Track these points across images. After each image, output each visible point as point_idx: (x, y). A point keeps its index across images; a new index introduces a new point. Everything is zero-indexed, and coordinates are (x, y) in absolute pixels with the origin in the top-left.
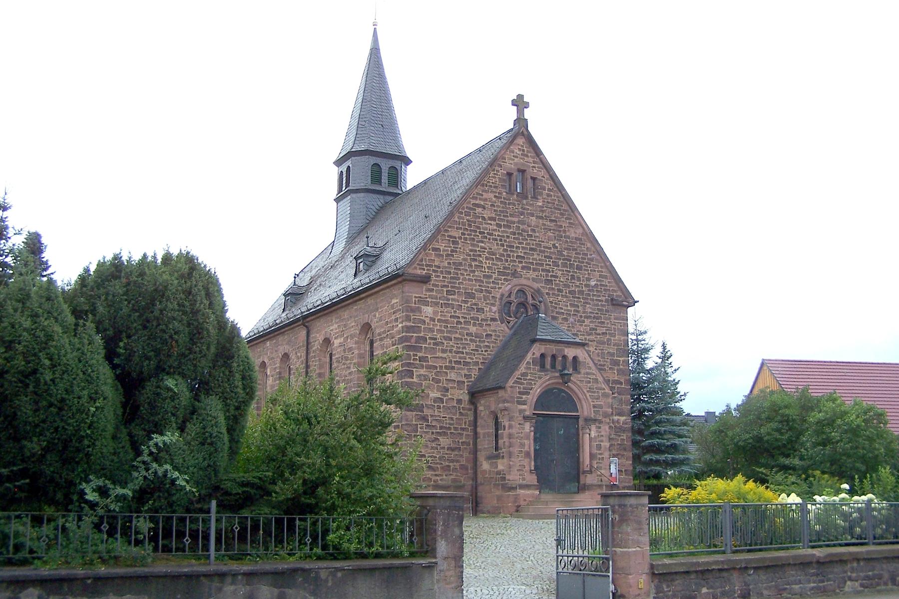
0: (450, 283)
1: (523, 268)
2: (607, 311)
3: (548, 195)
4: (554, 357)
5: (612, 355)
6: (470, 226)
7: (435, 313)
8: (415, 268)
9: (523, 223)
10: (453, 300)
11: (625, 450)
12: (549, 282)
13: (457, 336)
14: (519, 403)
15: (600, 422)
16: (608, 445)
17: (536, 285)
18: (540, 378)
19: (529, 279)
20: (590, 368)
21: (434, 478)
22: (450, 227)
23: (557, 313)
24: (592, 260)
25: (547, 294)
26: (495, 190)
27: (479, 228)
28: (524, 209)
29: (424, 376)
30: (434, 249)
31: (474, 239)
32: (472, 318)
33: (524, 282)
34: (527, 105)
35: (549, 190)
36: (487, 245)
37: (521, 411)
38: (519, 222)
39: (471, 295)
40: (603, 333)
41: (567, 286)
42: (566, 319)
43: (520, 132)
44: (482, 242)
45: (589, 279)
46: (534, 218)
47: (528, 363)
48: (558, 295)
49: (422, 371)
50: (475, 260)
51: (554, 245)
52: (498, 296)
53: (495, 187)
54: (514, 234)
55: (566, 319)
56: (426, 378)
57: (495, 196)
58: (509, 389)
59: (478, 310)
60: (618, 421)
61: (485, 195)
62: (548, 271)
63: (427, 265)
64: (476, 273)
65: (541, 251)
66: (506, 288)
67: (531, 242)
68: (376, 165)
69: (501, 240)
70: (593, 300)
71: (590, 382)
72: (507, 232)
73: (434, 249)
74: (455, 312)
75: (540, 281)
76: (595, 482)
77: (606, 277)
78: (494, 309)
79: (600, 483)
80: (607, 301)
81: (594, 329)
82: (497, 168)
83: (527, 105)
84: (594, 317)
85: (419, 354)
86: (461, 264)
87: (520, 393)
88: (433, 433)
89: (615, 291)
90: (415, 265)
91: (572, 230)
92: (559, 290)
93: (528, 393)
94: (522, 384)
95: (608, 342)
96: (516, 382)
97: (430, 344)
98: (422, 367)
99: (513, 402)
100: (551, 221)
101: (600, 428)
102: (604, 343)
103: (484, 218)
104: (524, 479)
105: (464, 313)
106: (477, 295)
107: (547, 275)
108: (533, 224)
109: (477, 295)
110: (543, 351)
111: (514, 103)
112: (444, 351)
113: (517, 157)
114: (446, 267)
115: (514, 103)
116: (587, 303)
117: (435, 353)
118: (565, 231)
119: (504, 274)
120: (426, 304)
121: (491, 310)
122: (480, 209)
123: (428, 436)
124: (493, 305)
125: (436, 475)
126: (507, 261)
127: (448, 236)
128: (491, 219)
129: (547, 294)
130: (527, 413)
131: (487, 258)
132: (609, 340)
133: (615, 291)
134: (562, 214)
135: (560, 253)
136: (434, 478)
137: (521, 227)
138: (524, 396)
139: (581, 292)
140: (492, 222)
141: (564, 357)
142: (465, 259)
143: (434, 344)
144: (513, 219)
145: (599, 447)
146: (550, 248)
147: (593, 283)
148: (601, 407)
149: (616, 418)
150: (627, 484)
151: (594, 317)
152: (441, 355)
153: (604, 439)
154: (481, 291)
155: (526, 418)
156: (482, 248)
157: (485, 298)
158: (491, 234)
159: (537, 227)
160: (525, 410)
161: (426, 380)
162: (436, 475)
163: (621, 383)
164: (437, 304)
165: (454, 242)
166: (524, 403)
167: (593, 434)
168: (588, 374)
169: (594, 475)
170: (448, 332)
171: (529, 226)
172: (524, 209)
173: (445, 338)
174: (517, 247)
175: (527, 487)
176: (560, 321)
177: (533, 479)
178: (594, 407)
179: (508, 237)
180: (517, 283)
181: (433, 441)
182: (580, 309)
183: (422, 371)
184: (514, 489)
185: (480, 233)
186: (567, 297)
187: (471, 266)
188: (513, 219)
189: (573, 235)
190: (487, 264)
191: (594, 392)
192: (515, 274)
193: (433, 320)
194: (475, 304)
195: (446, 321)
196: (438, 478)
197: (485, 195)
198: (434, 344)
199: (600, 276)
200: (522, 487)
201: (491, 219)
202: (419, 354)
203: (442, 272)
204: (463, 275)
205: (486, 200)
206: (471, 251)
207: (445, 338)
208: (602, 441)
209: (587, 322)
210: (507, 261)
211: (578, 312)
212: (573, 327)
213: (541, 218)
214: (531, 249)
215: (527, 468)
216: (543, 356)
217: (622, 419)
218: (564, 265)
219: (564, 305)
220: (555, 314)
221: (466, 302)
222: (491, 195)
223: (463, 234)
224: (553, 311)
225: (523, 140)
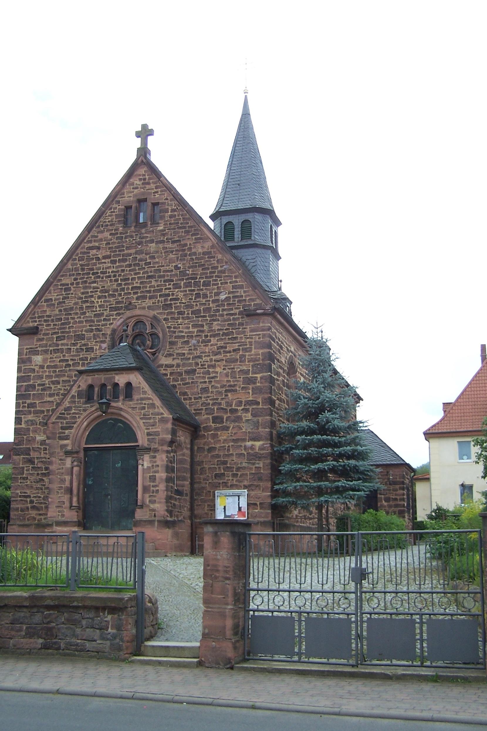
0: (61, 329)
1: (138, 299)
2: (241, 324)
3: (171, 217)
4: (103, 386)
5: (247, 372)
6: (83, 270)
7: (45, 360)
8: (28, 322)
9: (140, 252)
10: (62, 344)
11: (260, 479)
12: (167, 306)
13: (66, 378)
14: (61, 438)
15: (156, 450)
16: (164, 475)
17: (152, 313)
18: (85, 410)
19: (144, 309)
20: (145, 393)
21: (38, 517)
22: (62, 276)
23: (176, 337)
24: (223, 272)
25: (165, 319)
26: (110, 228)
27: (92, 269)
28: (143, 238)
29: (32, 421)
30: (47, 301)
31: (86, 282)
32: (81, 359)
33: (137, 312)
34: (151, 133)
35: (173, 210)
36: (99, 285)
37: (63, 446)
38: (136, 253)
39: (81, 337)
40: (234, 350)
41: (188, 306)
42: (187, 342)
43: (143, 162)
44: (95, 282)
45: (218, 294)
46: (154, 244)
47: (73, 397)
48: (179, 318)
49: (30, 417)
50: (87, 301)
51: (177, 268)
52: (109, 332)
53: (111, 225)
54: (130, 266)
55: (187, 342)
56: (33, 423)
57: (111, 234)
58: (51, 425)
59: (88, 350)
60: (252, 447)
61: (100, 236)
62: (168, 295)
63: (39, 317)
64: (87, 315)
65: (160, 277)
66: (118, 322)
67: (149, 270)
68: (229, 223)
69: (115, 276)
70: (222, 315)
71: (144, 408)
72: (122, 266)
73: (47, 301)
74: (64, 356)
75: (158, 307)
76: (146, 517)
77: (241, 287)
78: (104, 346)
79: (153, 518)
80: (240, 313)
81: (222, 347)
82: (115, 206)
83: (151, 133)
84: (224, 334)
85: (28, 401)
86: (72, 309)
87: (62, 428)
88: (38, 474)
89: (253, 300)
90: (28, 319)
91: (199, 246)
92: (180, 313)
93: (71, 428)
94: (65, 418)
95: (242, 359)
96: (58, 418)
97: (38, 390)
98: (30, 412)
99: (54, 439)
100: (174, 242)
101: (155, 457)
102: (236, 360)
103: (98, 259)
104: (63, 516)
105: (72, 356)
106: (87, 335)
107: (166, 300)
108: (152, 250)
109: (87, 335)
110: (90, 382)
111: (138, 135)
112: (51, 395)
113: (137, 188)
114: (57, 315)
115: (138, 135)
116: (214, 320)
117: (43, 399)
118: (190, 249)
119: (116, 309)
120: (36, 353)
121: (100, 348)
122: (94, 251)
123: (34, 477)
124: (102, 342)
125: (40, 515)
126: (120, 295)
127: (61, 285)
128: (104, 257)
129: (165, 319)
130: (69, 448)
131: (99, 297)
132: (242, 356)
133: (253, 300)
134: (186, 232)
135: (183, 273)
136: (38, 517)
137: (138, 257)
138: (67, 431)
139: (208, 310)
140: (107, 261)
141: (116, 385)
142: (76, 304)
143: (42, 390)
144: (130, 251)
145: (153, 479)
146: (172, 271)
147: (223, 297)
148: (157, 434)
149: (249, 444)
150: (262, 520)
151: (224, 334)
152: (49, 399)
153: (159, 469)
154: (92, 330)
155: (68, 453)
156: (94, 288)
157: (95, 336)
158: (105, 273)
159: (157, 252)
160: (66, 445)
161: (33, 424)
162: (40, 515)
163: (258, 403)
164: (46, 352)
165: (66, 290)
166: (67, 438)
167: (146, 465)
168: (142, 399)
169: (145, 509)
170: (57, 376)
171: (146, 254)
172: (143, 238)
173: (53, 383)
174: (133, 279)
175: (65, 523)
176: (179, 345)
177: (72, 516)
178: (148, 434)
179: (123, 271)
180: (130, 315)
181: (37, 482)
182: (206, 328)
183: (30, 417)
184: (50, 525)
185: (93, 274)
186: (188, 318)
187: (82, 308)
188: (130, 251)
189: (200, 250)
190: (97, 302)
191: (150, 418)
192: (129, 306)
193: (42, 367)
194: (84, 345)
195: (55, 366)
196: (42, 517)
197: (100, 236)
198: (42, 390)
199: (233, 287)
200: (59, 524)
201: (104, 257)
202: (28, 401)
203: (53, 321)
204: (73, 318)
205: (101, 240)
206: (83, 293)
207: (53, 383)
208: (157, 472)
209: (213, 341)
210: (120, 295)
211: (203, 331)
212: (196, 349)
213: (163, 242)
214: (149, 277)
215: (67, 504)
216: (91, 387)
217: (258, 444)
218: (187, 285)
219: (185, 327)
220: (173, 340)
221: (74, 345)
222: (107, 234)
223: (75, 279)
224: (171, 336)
225: (145, 169)
